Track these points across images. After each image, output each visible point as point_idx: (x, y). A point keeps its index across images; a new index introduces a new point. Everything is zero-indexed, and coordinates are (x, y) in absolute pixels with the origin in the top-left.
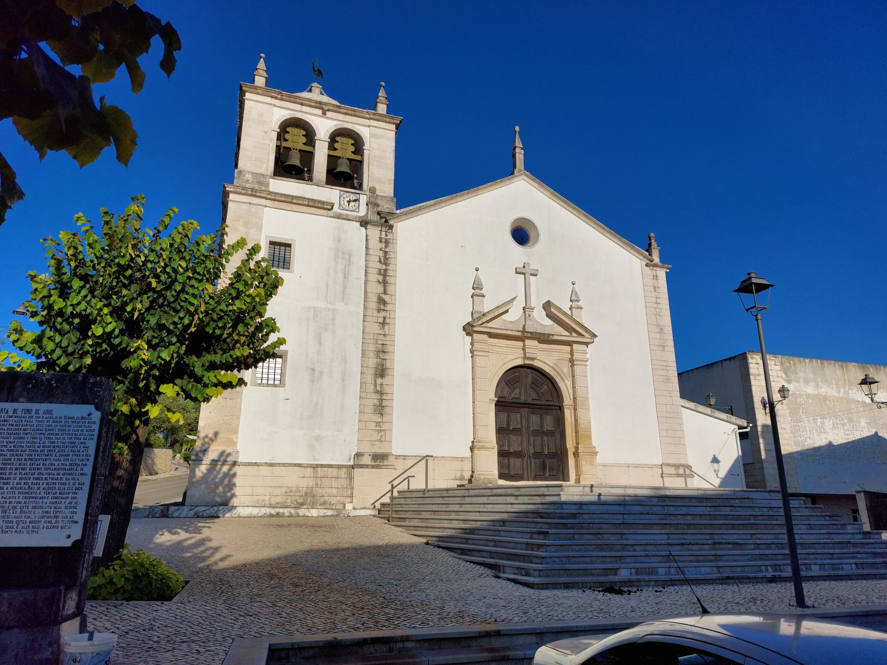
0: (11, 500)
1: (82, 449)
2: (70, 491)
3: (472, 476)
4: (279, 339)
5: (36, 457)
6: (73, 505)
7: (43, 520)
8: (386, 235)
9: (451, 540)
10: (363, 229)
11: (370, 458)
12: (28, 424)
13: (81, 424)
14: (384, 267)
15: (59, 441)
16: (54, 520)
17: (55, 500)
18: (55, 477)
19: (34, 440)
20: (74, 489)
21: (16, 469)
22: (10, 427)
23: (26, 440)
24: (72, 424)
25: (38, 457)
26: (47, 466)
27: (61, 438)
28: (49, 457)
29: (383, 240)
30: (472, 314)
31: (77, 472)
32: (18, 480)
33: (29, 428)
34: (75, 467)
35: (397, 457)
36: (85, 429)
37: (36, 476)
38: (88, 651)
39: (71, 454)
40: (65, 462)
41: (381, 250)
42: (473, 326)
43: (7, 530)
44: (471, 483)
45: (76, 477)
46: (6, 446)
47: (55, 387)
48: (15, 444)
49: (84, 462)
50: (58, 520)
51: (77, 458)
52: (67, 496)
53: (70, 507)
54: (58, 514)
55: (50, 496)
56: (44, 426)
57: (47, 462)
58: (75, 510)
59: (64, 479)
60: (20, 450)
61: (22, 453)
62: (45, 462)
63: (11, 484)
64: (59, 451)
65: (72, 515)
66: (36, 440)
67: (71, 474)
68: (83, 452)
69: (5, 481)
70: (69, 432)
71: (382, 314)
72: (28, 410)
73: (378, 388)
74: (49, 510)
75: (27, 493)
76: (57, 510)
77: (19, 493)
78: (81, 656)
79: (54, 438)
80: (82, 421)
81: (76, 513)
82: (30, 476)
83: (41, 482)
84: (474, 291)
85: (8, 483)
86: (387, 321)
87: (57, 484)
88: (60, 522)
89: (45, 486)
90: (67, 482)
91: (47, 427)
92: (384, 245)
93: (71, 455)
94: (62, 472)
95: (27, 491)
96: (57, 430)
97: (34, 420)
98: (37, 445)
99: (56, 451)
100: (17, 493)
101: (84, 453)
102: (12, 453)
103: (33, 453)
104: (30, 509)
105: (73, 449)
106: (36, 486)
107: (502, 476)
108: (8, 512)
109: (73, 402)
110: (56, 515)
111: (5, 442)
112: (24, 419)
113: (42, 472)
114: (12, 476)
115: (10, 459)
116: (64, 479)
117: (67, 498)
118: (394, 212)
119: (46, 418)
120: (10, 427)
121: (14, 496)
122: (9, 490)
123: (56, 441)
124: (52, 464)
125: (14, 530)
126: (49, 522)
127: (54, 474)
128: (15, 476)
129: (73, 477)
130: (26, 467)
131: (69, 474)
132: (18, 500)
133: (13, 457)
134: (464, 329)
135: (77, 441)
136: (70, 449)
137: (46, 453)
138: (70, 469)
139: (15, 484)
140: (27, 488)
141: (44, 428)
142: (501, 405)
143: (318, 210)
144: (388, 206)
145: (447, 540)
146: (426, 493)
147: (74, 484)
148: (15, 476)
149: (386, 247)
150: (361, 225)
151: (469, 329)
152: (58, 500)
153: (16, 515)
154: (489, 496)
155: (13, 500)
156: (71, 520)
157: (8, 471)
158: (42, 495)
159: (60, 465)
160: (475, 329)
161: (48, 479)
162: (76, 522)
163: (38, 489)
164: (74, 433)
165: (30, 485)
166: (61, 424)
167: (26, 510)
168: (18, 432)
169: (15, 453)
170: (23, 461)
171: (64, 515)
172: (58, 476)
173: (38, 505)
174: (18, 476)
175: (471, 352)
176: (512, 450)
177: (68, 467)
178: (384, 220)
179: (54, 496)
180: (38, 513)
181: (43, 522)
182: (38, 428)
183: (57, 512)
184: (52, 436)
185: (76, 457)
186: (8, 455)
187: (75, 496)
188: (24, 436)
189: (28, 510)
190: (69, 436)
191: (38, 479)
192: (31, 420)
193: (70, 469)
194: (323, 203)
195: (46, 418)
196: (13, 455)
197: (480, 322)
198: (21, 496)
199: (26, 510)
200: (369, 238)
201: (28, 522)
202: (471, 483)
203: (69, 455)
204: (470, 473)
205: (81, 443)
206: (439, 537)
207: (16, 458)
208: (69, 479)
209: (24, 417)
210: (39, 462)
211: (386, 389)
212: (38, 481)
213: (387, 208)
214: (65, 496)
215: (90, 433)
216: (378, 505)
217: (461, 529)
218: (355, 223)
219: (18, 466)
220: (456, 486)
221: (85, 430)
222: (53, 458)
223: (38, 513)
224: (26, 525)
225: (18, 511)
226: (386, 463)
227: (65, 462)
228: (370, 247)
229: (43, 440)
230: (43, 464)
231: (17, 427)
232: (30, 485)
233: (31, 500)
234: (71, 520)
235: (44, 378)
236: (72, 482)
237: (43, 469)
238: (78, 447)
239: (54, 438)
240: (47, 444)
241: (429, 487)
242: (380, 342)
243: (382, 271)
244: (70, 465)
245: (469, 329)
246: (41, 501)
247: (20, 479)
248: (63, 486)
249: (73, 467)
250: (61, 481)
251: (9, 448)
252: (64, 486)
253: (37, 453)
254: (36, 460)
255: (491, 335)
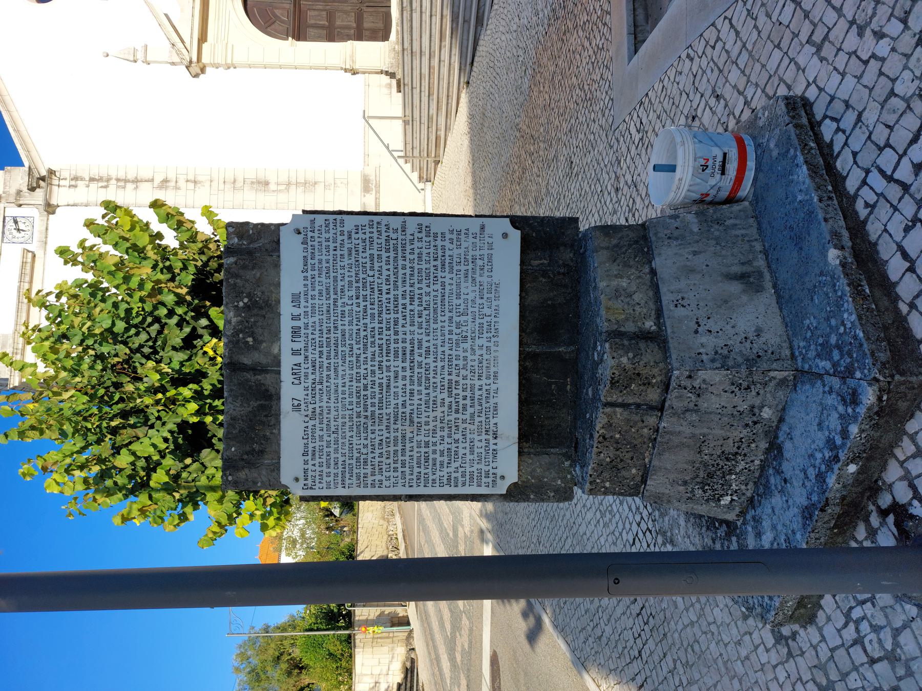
0: (447, 332)
1: (360, 235)
2: (433, 243)
3: (387, 73)
4: (203, 214)
5: (376, 306)
6: (454, 236)
7: (478, 279)
8: (66, 179)
9: (464, 50)
10: (58, 210)
11: (367, 195)
12: (318, 328)
13: (316, 243)
14: (113, 182)
15: (347, 274)
16: (479, 263)
17: (447, 265)
18: (408, 271)
19: (347, 315)
20: (428, 239)
21: (396, 333)
22: (324, 356)
23: (347, 328)
24: (317, 257)
25: (376, 303)
26: (392, 286)
27: (342, 271)
28: (376, 287)
29: (73, 183)
30: (173, 64)
31: (400, 237)
32: (415, 328)
33: (325, 325)
34: (392, 242)
35: (366, 164)
36: (324, 235)
37: (407, 301)
38: (691, 147)
39: (368, 252)
40: (384, 259)
41: (88, 186)
42: (191, 62)
43: (493, 330)
44: (394, 73)
45: (409, 237)
46: (358, 356)
47: (250, 300)
48: (354, 342)
49: (384, 229)
50: (478, 257)
51: (376, 241)
52: (440, 248)
53: (458, 240)
54: (470, 258)
55: (440, 274)
56: (321, 302)
57: (384, 288)
58: (463, 231)
59: (412, 257)
60: (365, 333)
61: (369, 330)
62: (384, 291)
63: (420, 337)
64: (365, 272)
65: (471, 236)
66: (347, 312)
67: (404, 246)
68: (365, 233)
69: (416, 347)
70: (331, 261)
71: (182, 183)
72: (294, 332)
73: (283, 187)
74: (462, 273)
75: (435, 310)
76: (463, 260)
77: (435, 322)
78: (700, 158)
79: (342, 283)
80: (310, 243)
81: (468, 230)
82: (408, 310)
83: (417, 292)
84: (139, 62)
85: (420, 342)
86: (191, 177)
87: (420, 266)
88: (482, 252)
89: (423, 285)
90: (417, 251)
91: (324, 298)
92: (79, 183)
93: (371, 252)
94: (400, 262)
95: (432, 311)
96: (328, 281)
97: (311, 320)
98: (355, 308)
99: (365, 276)
100: (435, 326)
101: (368, 230)
102: (369, 344)
103: (369, 311)
104: (461, 301)
105: (361, 250)
106: (425, 298)
107: (385, 37)
108: (464, 334)
109: (277, 265)
110: (470, 260)
111: (351, 359)
112: (310, 337)
113: (400, 293)
114: (409, 337)
115: (380, 346)
116: (412, 257)
117: (443, 247)
118: (27, 169)
119: (307, 302)
120: (324, 356)
121: (439, 328)
122: (430, 338)
123: (347, 279)
124: (387, 280)
125: (494, 319)
126: (482, 269)
127: (405, 274)
128: (408, 333)
129: (408, 244)
130: (392, 320)
131: (404, 250)
132: (447, 321)
133: (377, 341)
134: (196, 76)
135: (347, 246)
136: (361, 254)
137: (368, 292)
138: (395, 249)
139: (420, 331)
140: (427, 312)
141: (325, 302)
142: (299, 34)
143: (36, 270)
144: (20, 178)
145: (464, 55)
146: (407, 118)
147: (420, 240)
148: (408, 333)
149: (82, 179)
150: (53, 213)
151: (197, 68)
152: (447, 261)
153: (470, 320)
154: (412, 10)
155: (447, 329)
156: (478, 235)
157: (400, 345)
158: (438, 287)
159: (388, 267)
160: (195, 59)
161: (412, 281)
162: (483, 228)
163: (428, 294)
164: (332, 252)
165: (422, 308)
166: (317, 276)
167: (462, 307)
168: (333, 342)
169: (370, 340)
170: (384, 325)
171: (470, 248)
172: (408, 267)
173: (454, 290)
174: (408, 328)
175: (229, 68)
176: (355, 25)
177: (392, 254)
178: (42, 183)
179: (439, 269)
180: (468, 289)
181: (482, 279)
182: (325, 312)
183: (466, 260)
184: (339, 288)
185: (375, 243)
186: (373, 350)
187: (439, 235)
188: (339, 331)
189: (463, 305)
190: (339, 259)
191: (412, 299)
192: (310, 324)
193: (395, 249)
194: (24, 263)
195: (307, 302)
196: (373, 343)
197: (184, 51)
198: (440, 318)
199: (462, 307)
200: (71, 203)
201: (481, 301)
202: (394, 73)
203: (372, 255)
204: (383, 76)
205: (350, 238)
206: (460, 69)
207: (377, 336)
208: (413, 249)
209: (307, 337)
210: (384, 301)
211: (284, 178)
212: (417, 296)
213: (22, 178)
214: (440, 253)
215: (331, 226)
216: (421, 186)
217: (452, 38)
218: (50, 222)
219: (392, 332)
220: (400, 95)
221: (327, 236)
222: (377, 280)
223: (468, 289)
224: (486, 303)
225: (463, 318)
226: (372, 177)
227: (384, 259)
228: (85, 201)
229: (346, 300)
230: (387, 293)
231: (325, 345)
232: (422, 308)
233: (447, 304)
234: (478, 235)
235: (234, 320)
236: (417, 244)
237: (396, 292)
238: (357, 242)
239: (342, 283)
240: (353, 293)
241: (400, 113)
242: (222, 186)
243: (119, 184)
244: (388, 251)
245: (197, 68)
246: (448, 287)
247: (412, 325)
248: (424, 257)
249: (391, 246)
250: (416, 261)
251: (362, 351)
252: (424, 255)
253: (369, 307)
254: (380, 306)
255: (203, 38)
